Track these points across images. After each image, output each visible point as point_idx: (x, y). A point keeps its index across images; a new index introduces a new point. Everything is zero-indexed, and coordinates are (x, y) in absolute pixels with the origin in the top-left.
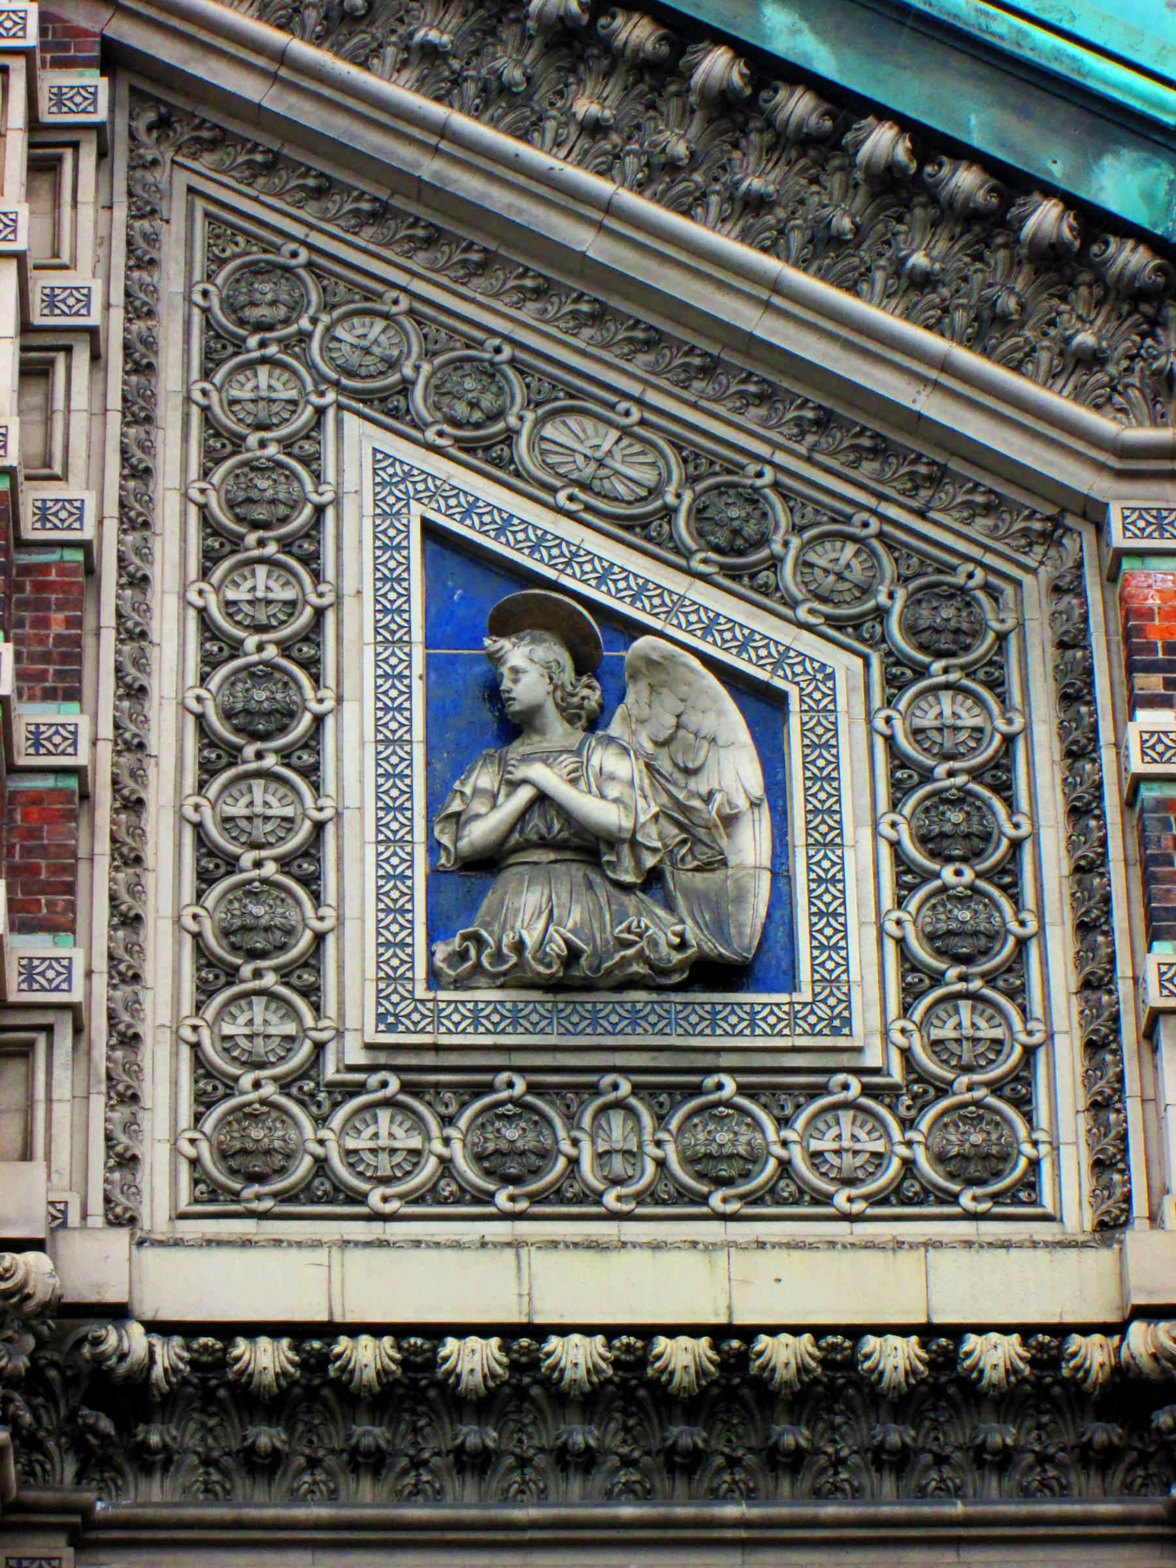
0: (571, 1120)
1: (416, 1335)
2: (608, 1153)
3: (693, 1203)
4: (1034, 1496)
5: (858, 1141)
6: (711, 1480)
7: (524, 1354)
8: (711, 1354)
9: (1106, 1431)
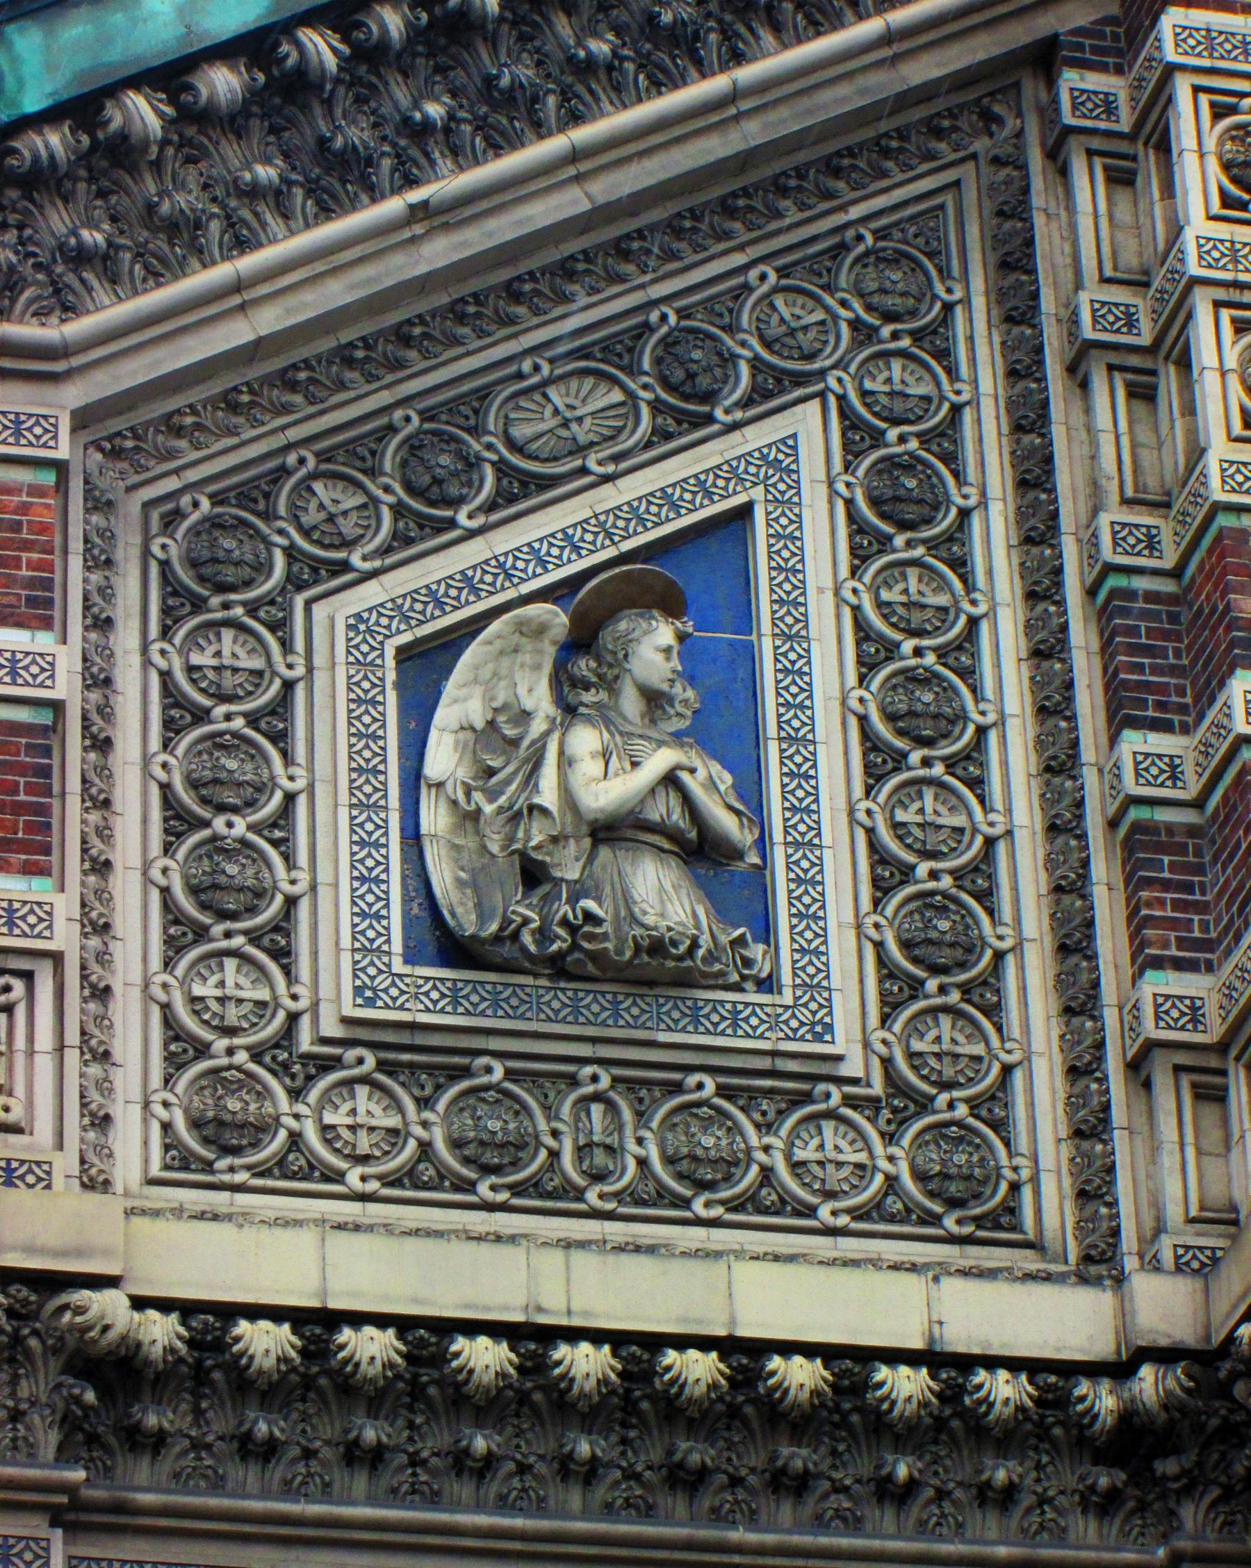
0: (550, 1112)
1: (316, 1323)
2: (590, 1145)
3: (674, 1206)
4: (828, 1526)
5: (841, 1151)
6: (392, 1477)
7: (314, 1343)
8: (295, 1340)
9: (1109, 1474)
